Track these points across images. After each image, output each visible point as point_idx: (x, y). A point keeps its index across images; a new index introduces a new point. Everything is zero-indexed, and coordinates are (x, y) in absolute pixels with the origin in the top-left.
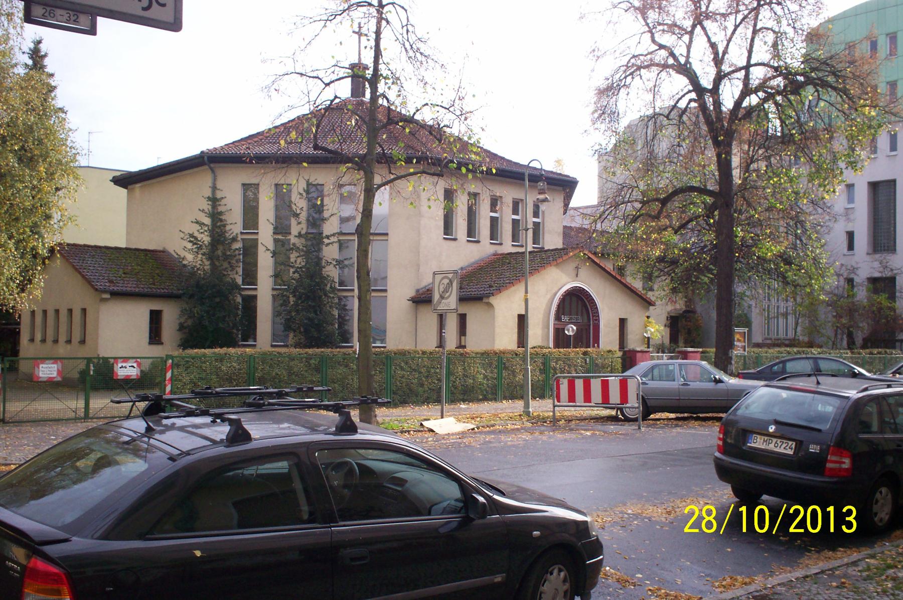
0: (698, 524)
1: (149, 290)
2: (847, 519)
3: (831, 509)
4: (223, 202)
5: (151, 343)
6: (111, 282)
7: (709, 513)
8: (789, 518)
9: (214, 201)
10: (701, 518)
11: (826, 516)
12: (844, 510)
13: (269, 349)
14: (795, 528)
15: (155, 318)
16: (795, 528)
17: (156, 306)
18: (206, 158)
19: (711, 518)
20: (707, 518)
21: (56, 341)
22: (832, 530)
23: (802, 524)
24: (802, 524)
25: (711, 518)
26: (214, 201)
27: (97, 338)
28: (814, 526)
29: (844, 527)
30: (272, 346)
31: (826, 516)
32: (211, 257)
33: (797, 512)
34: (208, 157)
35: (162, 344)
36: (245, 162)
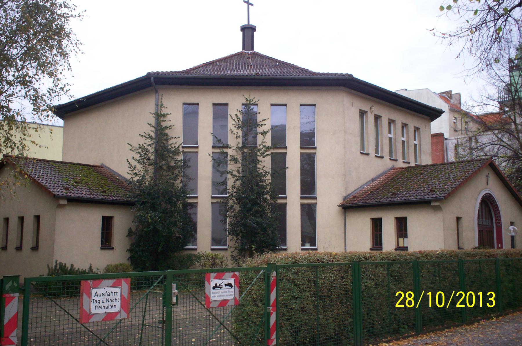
0: (403, 302)
1: (103, 197)
2: (490, 299)
3: (480, 293)
4: (168, 118)
5: (102, 248)
6: (67, 189)
7: (410, 296)
8: (456, 299)
9: (159, 116)
10: (405, 298)
11: (478, 297)
12: (488, 294)
13: (209, 251)
14: (459, 305)
15: (107, 222)
16: (459, 305)
17: (108, 212)
18: (152, 78)
19: (411, 299)
20: (409, 299)
21: (19, 248)
22: (481, 306)
23: (464, 302)
24: (464, 302)
25: (409, 299)
26: (159, 116)
27: (53, 244)
28: (471, 303)
29: (488, 304)
30: (212, 250)
31: (478, 297)
32: (158, 169)
33: (461, 295)
34: (155, 78)
35: (113, 249)
36: (77, 109)
